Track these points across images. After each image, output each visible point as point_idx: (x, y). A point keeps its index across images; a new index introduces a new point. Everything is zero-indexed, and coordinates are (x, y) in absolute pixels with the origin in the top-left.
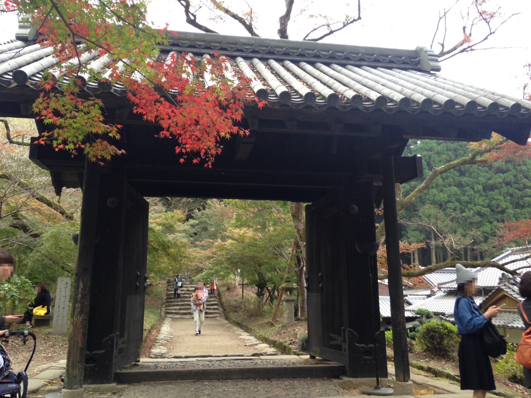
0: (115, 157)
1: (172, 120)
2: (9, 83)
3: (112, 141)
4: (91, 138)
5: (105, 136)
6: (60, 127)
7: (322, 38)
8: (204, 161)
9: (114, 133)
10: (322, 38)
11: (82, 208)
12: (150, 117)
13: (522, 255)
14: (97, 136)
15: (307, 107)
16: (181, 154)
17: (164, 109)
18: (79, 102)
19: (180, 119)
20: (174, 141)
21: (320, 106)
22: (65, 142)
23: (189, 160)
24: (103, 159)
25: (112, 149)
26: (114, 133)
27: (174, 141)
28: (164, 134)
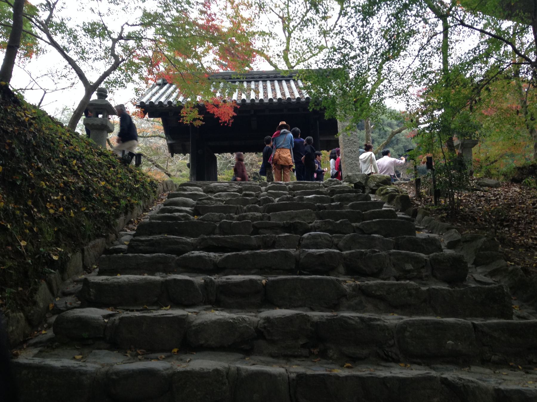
0: (202, 125)
1: (217, 112)
2: (166, 105)
3: (201, 120)
4: (195, 120)
5: (199, 119)
6: (186, 117)
7: (46, 42)
8: (228, 124)
9: (201, 118)
10: (46, 42)
11: (136, 132)
12: (212, 112)
13: (191, 255)
14: (197, 119)
15: (271, 104)
16: (221, 123)
17: (215, 109)
18: (498, 179)
19: (220, 112)
20: (218, 118)
21: (275, 103)
22: (187, 121)
23: (224, 124)
24: (199, 126)
25: (201, 122)
26: (201, 118)
27: (218, 118)
28: (216, 117)
